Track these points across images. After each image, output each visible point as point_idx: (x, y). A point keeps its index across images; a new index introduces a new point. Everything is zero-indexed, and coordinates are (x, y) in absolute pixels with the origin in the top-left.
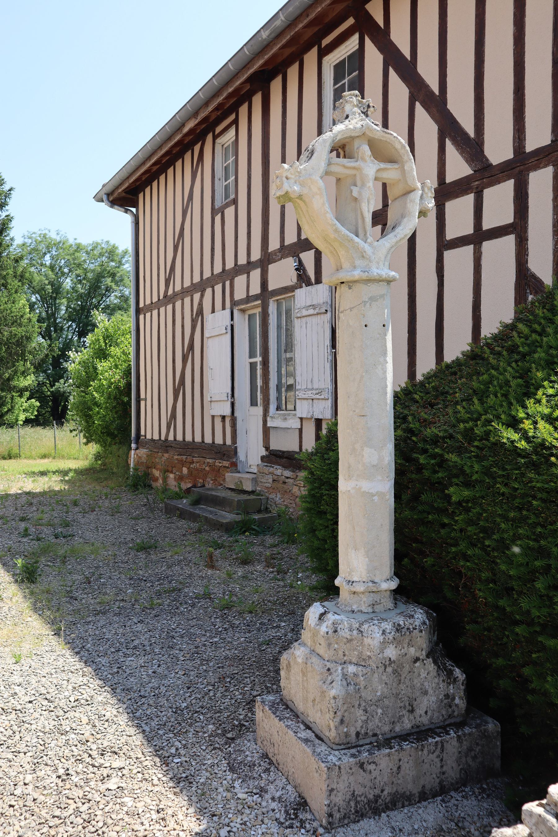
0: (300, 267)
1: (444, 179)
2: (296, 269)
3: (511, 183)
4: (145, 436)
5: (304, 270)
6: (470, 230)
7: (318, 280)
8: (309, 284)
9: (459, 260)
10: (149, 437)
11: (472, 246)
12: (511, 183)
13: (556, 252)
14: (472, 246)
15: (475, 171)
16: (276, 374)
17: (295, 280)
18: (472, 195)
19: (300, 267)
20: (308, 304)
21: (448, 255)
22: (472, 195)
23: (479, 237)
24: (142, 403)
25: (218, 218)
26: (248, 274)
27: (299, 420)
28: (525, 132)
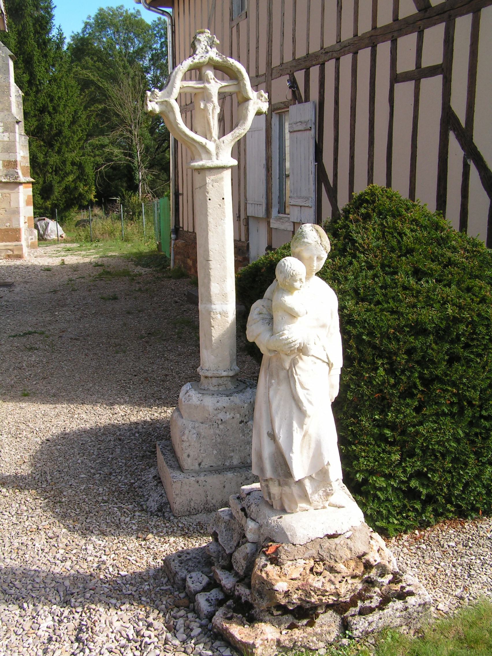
0: (293, 84)
1: (397, 16)
2: (290, 88)
3: (443, 25)
4: (183, 228)
5: (298, 88)
6: (412, 67)
7: (307, 100)
8: (300, 102)
9: (404, 91)
10: (185, 229)
11: (414, 81)
12: (443, 25)
13: (489, 230)
14: (414, 81)
15: (419, 11)
16: (278, 180)
17: (290, 97)
18: (416, 33)
19: (293, 84)
20: (298, 121)
21: (398, 87)
22: (416, 33)
23: (419, 74)
24: (181, 197)
25: (234, 30)
26: (374, 28)
27: (292, 224)
28: (481, 178)
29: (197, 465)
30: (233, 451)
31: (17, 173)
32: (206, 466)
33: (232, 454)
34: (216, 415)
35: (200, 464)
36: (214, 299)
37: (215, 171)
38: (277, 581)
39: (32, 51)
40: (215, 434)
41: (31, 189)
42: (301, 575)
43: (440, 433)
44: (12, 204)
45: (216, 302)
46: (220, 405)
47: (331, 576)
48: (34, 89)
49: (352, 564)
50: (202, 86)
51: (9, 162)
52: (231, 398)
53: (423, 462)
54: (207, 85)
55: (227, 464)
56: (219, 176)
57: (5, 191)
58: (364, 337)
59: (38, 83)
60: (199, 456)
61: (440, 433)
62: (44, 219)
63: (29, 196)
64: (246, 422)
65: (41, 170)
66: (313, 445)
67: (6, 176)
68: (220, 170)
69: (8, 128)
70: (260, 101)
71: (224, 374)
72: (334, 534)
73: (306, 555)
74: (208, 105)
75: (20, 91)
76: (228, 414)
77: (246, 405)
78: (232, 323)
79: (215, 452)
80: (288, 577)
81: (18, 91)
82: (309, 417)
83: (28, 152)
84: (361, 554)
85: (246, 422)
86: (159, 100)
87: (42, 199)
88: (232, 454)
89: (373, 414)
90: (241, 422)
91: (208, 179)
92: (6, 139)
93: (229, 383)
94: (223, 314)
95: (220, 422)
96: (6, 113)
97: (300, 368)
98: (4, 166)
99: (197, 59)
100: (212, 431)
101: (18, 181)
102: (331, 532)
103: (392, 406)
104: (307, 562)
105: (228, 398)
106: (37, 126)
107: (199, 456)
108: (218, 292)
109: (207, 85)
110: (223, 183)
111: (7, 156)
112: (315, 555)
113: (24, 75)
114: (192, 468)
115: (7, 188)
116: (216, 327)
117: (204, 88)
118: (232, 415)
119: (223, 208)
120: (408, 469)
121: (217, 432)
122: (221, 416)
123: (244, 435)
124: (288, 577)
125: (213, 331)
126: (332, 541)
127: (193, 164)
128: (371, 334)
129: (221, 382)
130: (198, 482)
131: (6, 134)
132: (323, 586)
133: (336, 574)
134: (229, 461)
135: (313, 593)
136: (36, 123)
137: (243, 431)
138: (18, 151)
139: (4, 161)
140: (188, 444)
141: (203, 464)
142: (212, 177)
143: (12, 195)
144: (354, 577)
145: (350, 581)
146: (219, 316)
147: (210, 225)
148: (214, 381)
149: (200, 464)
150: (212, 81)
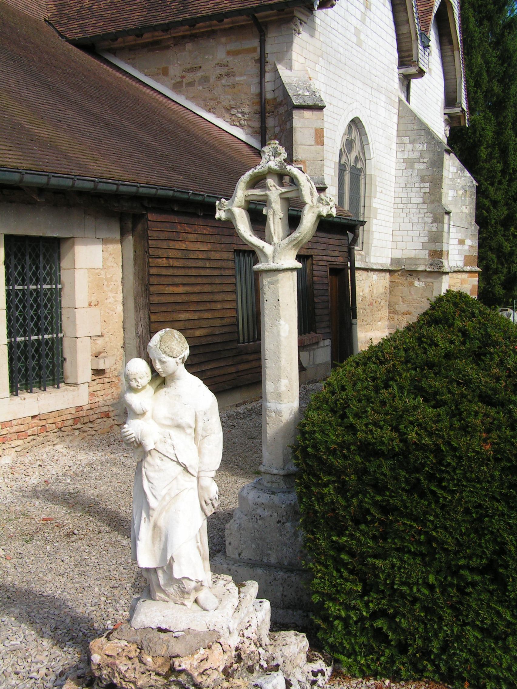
29: (237, 555)
30: (271, 549)
31: (442, 262)
32: (246, 558)
33: (270, 552)
34: (254, 510)
35: (240, 555)
36: (269, 397)
37: (271, 273)
38: (94, 652)
39: (508, 141)
40: (254, 528)
41: (477, 279)
42: (118, 654)
43: (404, 573)
44: (434, 292)
45: (270, 401)
46: (259, 500)
47: (138, 665)
48: (507, 178)
49: (160, 661)
50: (264, 193)
51: (435, 251)
52: (272, 496)
53: (390, 601)
54: (268, 192)
55: (265, 560)
56: (275, 278)
57: (429, 280)
58: (309, 449)
59: (511, 171)
60: (239, 546)
61: (404, 573)
62: (507, 310)
63: (473, 286)
64: (283, 523)
65: (507, 261)
66: (163, 539)
67: (431, 265)
68: (276, 273)
69: (437, 218)
70: (321, 205)
71: (275, 472)
72: (166, 629)
73: (131, 639)
74: (269, 211)
75: (474, 182)
76: (266, 511)
77: (284, 505)
78: (287, 424)
79: (254, 546)
80: (103, 652)
81: (472, 182)
82: (153, 509)
83: (477, 241)
84: (173, 655)
85: (283, 523)
86: (226, 208)
87: (503, 289)
88: (270, 552)
89: (330, 536)
90: (279, 522)
91: (265, 281)
92: (434, 229)
93: (282, 482)
94: (278, 413)
95: (258, 518)
96: (436, 204)
97: (147, 462)
98: (430, 255)
99: (259, 169)
100: (251, 525)
101: (442, 270)
102: (164, 626)
103: (347, 529)
104: (129, 645)
105: (268, 495)
106: (508, 215)
107: (239, 546)
108: (272, 391)
109: (268, 192)
110: (279, 285)
111: (434, 246)
112: (139, 642)
113: (498, 165)
114: (232, 556)
115: (430, 277)
116: (270, 424)
117: (266, 195)
118: (270, 513)
119: (278, 309)
120: (371, 605)
121: (256, 526)
122: (259, 511)
123: (281, 536)
124: (103, 652)
125: (268, 428)
126: (162, 635)
127: (256, 267)
128: (314, 447)
129: (274, 479)
130: (230, 570)
131: (435, 225)
132: (126, 671)
133: (142, 665)
134: (266, 558)
135: (117, 675)
136: (506, 212)
137: (280, 531)
138: (444, 241)
139: (430, 251)
140: (229, 532)
141: (243, 555)
142: (268, 279)
143: (435, 284)
144: (158, 674)
145: (154, 677)
146: (273, 414)
147: (266, 325)
148: (268, 477)
149: (240, 555)
150: (273, 189)
